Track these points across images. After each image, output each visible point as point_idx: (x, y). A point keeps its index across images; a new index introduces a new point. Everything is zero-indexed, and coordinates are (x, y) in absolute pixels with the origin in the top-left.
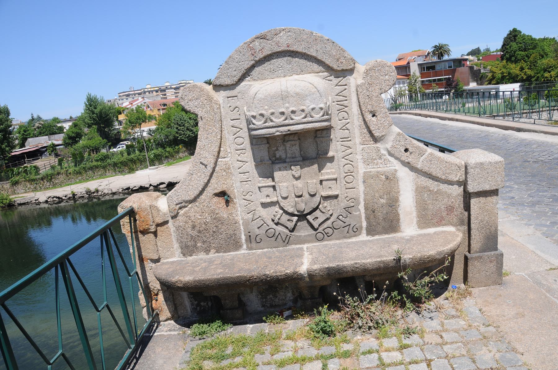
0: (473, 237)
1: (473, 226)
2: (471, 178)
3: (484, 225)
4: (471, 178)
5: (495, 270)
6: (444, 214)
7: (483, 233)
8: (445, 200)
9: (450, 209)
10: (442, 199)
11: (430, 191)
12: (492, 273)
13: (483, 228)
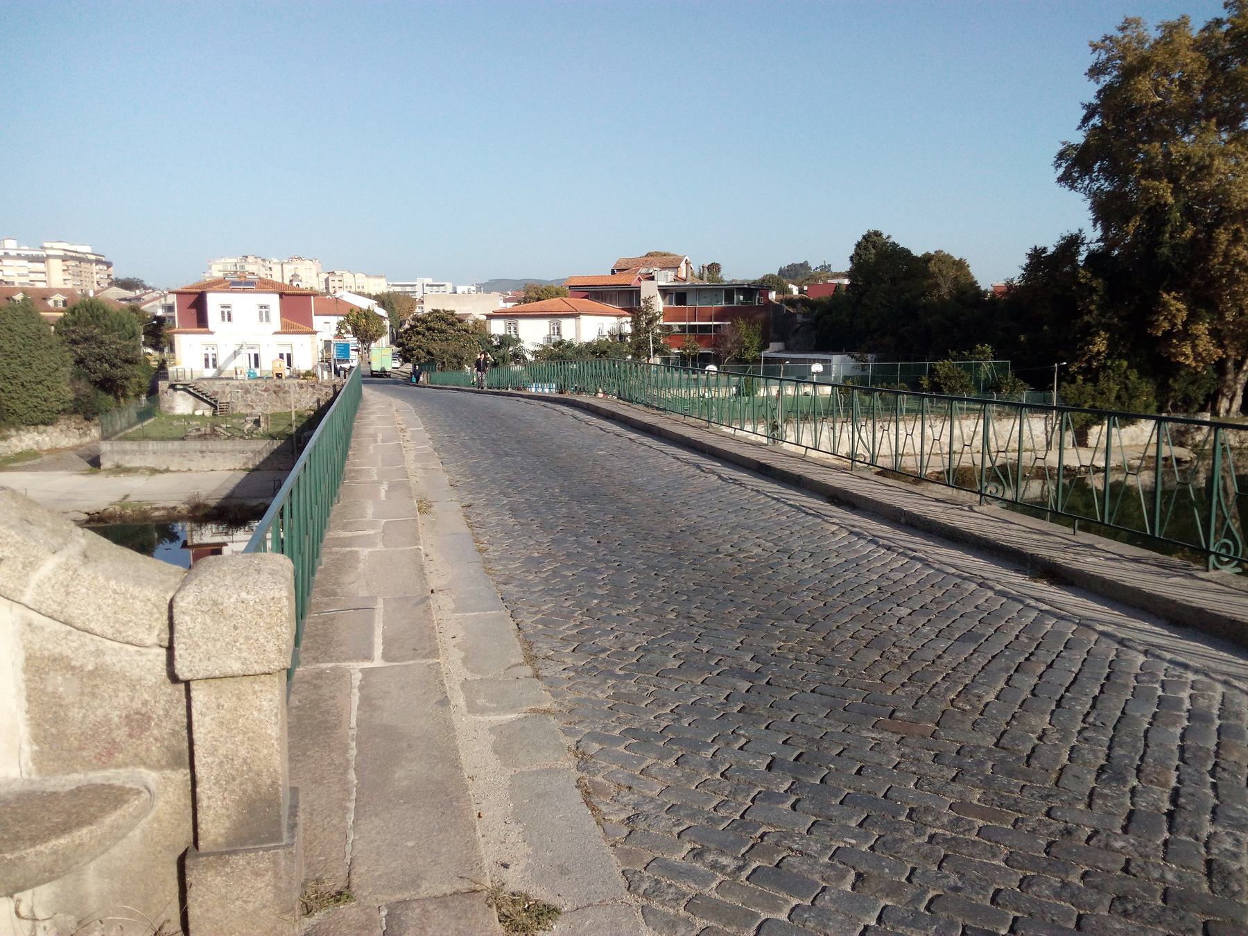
0: (203, 803)
1: (200, 771)
2: (183, 640)
3: (238, 771)
4: (183, 640)
5: (270, 896)
6: (121, 734)
7: (233, 791)
8: (121, 694)
9: (138, 722)
10: (112, 693)
11: (73, 668)
12: (264, 907)
13: (234, 779)
